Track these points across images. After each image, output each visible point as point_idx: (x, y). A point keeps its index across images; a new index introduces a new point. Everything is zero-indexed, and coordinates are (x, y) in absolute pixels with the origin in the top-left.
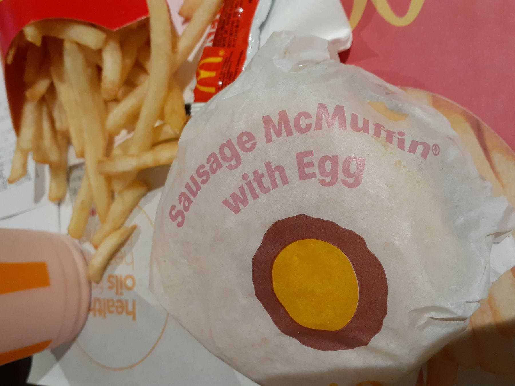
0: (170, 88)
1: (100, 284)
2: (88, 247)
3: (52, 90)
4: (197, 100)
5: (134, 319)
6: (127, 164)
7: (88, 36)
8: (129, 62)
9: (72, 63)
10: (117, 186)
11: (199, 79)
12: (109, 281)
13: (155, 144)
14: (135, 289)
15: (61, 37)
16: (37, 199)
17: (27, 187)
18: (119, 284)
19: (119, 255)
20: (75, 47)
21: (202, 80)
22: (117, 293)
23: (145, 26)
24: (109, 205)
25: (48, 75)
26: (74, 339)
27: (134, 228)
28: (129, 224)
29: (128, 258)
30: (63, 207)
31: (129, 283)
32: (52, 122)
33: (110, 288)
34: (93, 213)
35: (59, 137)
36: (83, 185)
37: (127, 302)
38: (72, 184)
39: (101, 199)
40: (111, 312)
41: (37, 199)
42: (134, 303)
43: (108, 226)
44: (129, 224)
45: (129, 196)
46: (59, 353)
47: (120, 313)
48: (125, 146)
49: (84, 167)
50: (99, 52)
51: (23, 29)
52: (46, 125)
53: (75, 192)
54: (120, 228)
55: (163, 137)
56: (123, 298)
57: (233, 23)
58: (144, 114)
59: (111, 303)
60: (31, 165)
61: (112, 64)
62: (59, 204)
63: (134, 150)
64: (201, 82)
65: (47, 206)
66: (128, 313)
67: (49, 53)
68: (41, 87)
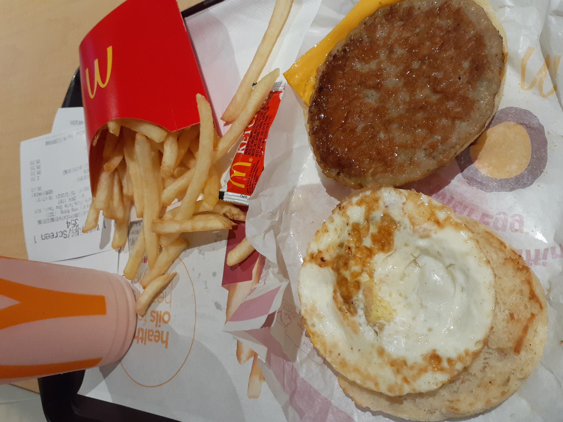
0: (210, 175)
1: (144, 318)
2: (138, 286)
3: (123, 165)
4: (229, 190)
5: (166, 347)
6: (173, 228)
7: (155, 133)
8: (183, 151)
9: (141, 149)
10: (164, 242)
11: (232, 176)
12: (152, 315)
13: (195, 214)
14: (169, 323)
15: (134, 129)
16: (102, 245)
17: (97, 235)
18: (159, 319)
19: (161, 295)
20: (144, 138)
21: (235, 177)
22: (156, 326)
23: (197, 127)
24: (157, 256)
25: (121, 153)
26: (120, 361)
27: (175, 275)
28: (171, 271)
29: (168, 298)
30: (122, 254)
31: (166, 318)
32: (121, 188)
33: (152, 321)
34: (145, 260)
35: (125, 199)
36: (140, 237)
37: (163, 332)
38: (131, 236)
39: (151, 251)
40: (150, 340)
41: (102, 245)
42: (168, 333)
43: (155, 272)
44: (171, 271)
45: (173, 250)
46: (106, 372)
47: (157, 341)
48: (174, 212)
49: (142, 223)
50: (162, 144)
51: (107, 125)
52: (116, 190)
53: (133, 242)
54: (163, 274)
55: (201, 209)
56: (159, 329)
57: (261, 139)
58: (189, 191)
59: (151, 333)
60: (101, 218)
61: (170, 153)
62: (119, 252)
63: (179, 217)
64: (234, 179)
65: (110, 252)
66: (163, 342)
67: (126, 139)
68: (116, 161)
